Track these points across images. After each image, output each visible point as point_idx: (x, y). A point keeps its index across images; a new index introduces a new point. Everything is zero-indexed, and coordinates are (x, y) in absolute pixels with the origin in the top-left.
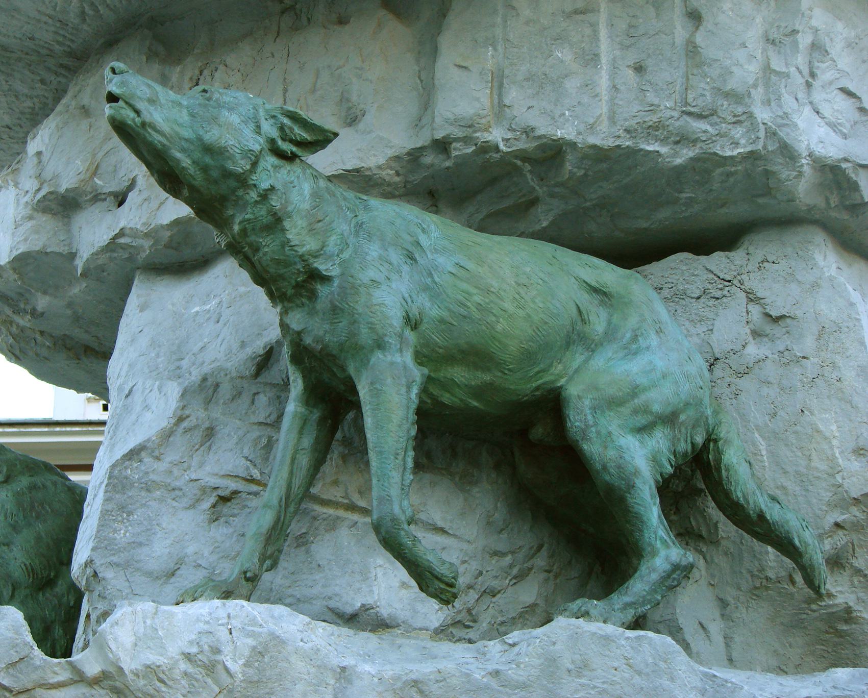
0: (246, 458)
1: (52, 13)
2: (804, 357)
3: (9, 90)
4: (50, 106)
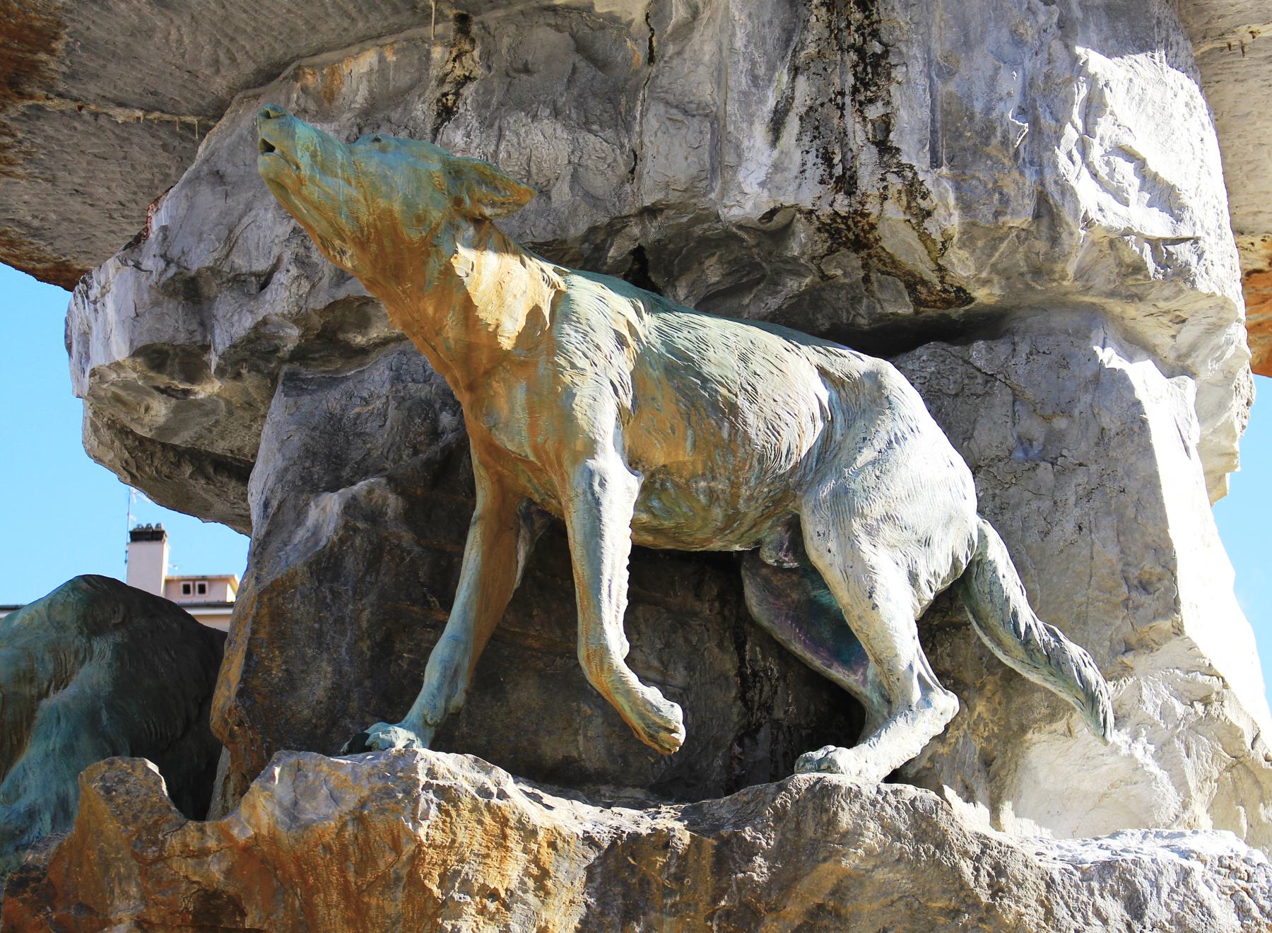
1: (180, 62)
2: (1080, 465)
3: (125, 158)
4: (173, 178)
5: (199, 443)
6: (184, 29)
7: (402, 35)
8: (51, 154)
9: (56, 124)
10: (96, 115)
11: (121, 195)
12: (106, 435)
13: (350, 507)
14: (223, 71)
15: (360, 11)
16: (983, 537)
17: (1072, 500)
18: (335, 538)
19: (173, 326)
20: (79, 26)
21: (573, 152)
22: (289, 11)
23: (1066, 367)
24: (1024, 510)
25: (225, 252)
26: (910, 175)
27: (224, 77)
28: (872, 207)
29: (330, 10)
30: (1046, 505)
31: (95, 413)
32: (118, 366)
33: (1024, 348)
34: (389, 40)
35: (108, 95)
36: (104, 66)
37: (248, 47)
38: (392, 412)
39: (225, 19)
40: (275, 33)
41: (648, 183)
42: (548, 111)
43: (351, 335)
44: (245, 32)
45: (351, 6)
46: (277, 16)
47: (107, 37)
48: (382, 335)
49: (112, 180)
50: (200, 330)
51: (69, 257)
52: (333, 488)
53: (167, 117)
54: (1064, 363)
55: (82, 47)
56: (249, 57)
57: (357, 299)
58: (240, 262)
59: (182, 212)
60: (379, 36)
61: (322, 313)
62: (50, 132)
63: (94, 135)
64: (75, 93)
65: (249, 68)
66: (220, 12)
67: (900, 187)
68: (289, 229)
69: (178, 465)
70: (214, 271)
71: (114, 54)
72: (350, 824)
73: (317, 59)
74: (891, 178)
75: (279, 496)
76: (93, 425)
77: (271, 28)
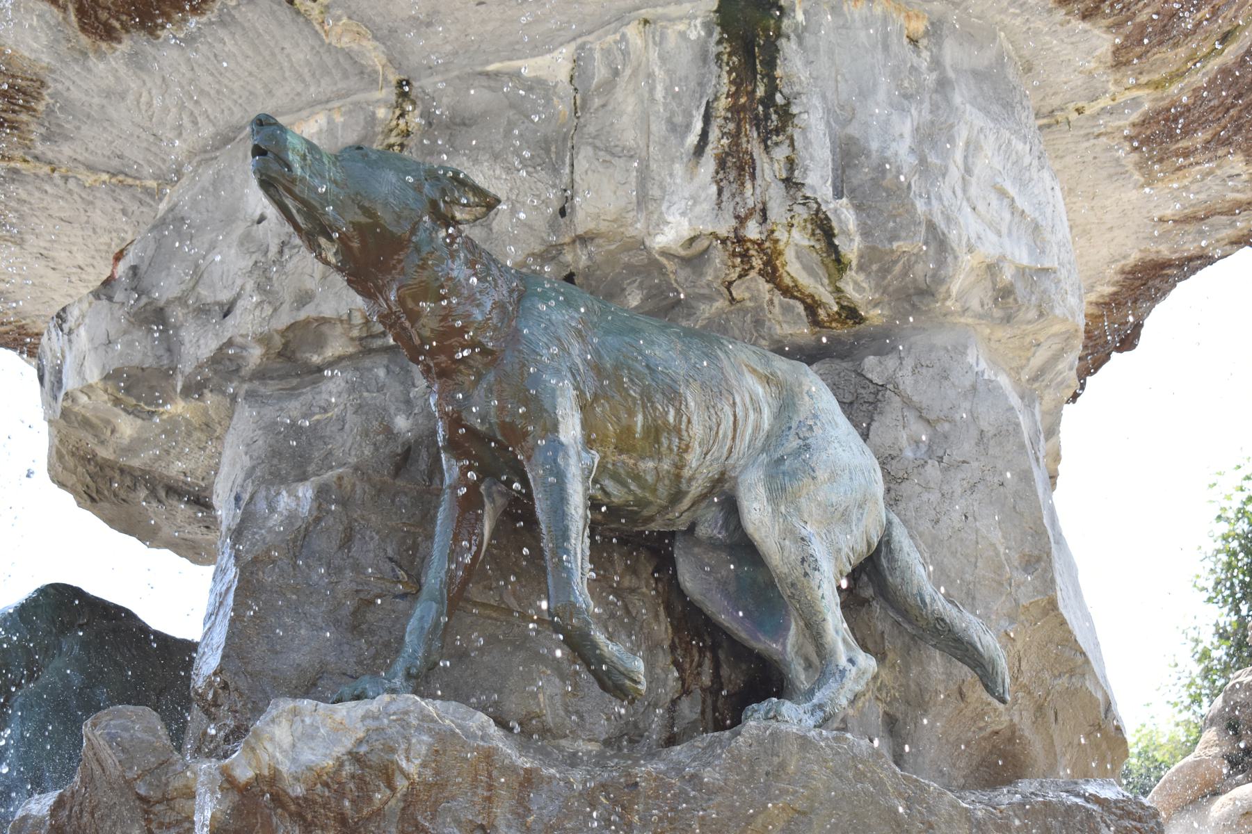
0: (391, 559)
1: (148, 124)
2: (964, 462)
3: (87, 222)
5: (156, 465)
6: (154, 92)
7: (349, 100)
8: (22, 217)
9: (29, 187)
10: (66, 179)
11: (80, 259)
12: (71, 462)
13: (322, 493)
15: (313, 75)
16: (889, 523)
17: (959, 491)
18: (310, 519)
19: (139, 350)
20: (59, 86)
21: (511, 190)
22: (251, 74)
23: (946, 378)
24: (917, 502)
25: (191, 284)
26: (815, 206)
27: (185, 141)
28: (781, 234)
29: (287, 74)
30: (934, 497)
31: (61, 441)
32: (88, 390)
33: (909, 363)
34: (336, 104)
35: (80, 158)
36: (78, 128)
37: (210, 111)
38: (350, 417)
39: (191, 82)
40: (235, 97)
41: (580, 215)
42: (487, 156)
43: (308, 355)
44: (209, 95)
45: (306, 70)
46: (240, 79)
47: (84, 98)
48: (337, 354)
49: (73, 244)
50: (167, 355)
51: (28, 321)
52: (303, 478)
53: (130, 181)
54: (944, 375)
55: (61, 108)
56: (210, 120)
57: (316, 320)
59: (150, 253)
60: (328, 101)
61: (283, 333)
62: (24, 195)
63: (62, 198)
64: (50, 155)
65: (207, 131)
66: (189, 75)
67: (805, 216)
68: (251, 263)
69: (133, 488)
70: (181, 300)
71: (89, 116)
72: (347, 763)
74: (798, 209)
75: (250, 489)
76: (59, 452)
77: (232, 91)
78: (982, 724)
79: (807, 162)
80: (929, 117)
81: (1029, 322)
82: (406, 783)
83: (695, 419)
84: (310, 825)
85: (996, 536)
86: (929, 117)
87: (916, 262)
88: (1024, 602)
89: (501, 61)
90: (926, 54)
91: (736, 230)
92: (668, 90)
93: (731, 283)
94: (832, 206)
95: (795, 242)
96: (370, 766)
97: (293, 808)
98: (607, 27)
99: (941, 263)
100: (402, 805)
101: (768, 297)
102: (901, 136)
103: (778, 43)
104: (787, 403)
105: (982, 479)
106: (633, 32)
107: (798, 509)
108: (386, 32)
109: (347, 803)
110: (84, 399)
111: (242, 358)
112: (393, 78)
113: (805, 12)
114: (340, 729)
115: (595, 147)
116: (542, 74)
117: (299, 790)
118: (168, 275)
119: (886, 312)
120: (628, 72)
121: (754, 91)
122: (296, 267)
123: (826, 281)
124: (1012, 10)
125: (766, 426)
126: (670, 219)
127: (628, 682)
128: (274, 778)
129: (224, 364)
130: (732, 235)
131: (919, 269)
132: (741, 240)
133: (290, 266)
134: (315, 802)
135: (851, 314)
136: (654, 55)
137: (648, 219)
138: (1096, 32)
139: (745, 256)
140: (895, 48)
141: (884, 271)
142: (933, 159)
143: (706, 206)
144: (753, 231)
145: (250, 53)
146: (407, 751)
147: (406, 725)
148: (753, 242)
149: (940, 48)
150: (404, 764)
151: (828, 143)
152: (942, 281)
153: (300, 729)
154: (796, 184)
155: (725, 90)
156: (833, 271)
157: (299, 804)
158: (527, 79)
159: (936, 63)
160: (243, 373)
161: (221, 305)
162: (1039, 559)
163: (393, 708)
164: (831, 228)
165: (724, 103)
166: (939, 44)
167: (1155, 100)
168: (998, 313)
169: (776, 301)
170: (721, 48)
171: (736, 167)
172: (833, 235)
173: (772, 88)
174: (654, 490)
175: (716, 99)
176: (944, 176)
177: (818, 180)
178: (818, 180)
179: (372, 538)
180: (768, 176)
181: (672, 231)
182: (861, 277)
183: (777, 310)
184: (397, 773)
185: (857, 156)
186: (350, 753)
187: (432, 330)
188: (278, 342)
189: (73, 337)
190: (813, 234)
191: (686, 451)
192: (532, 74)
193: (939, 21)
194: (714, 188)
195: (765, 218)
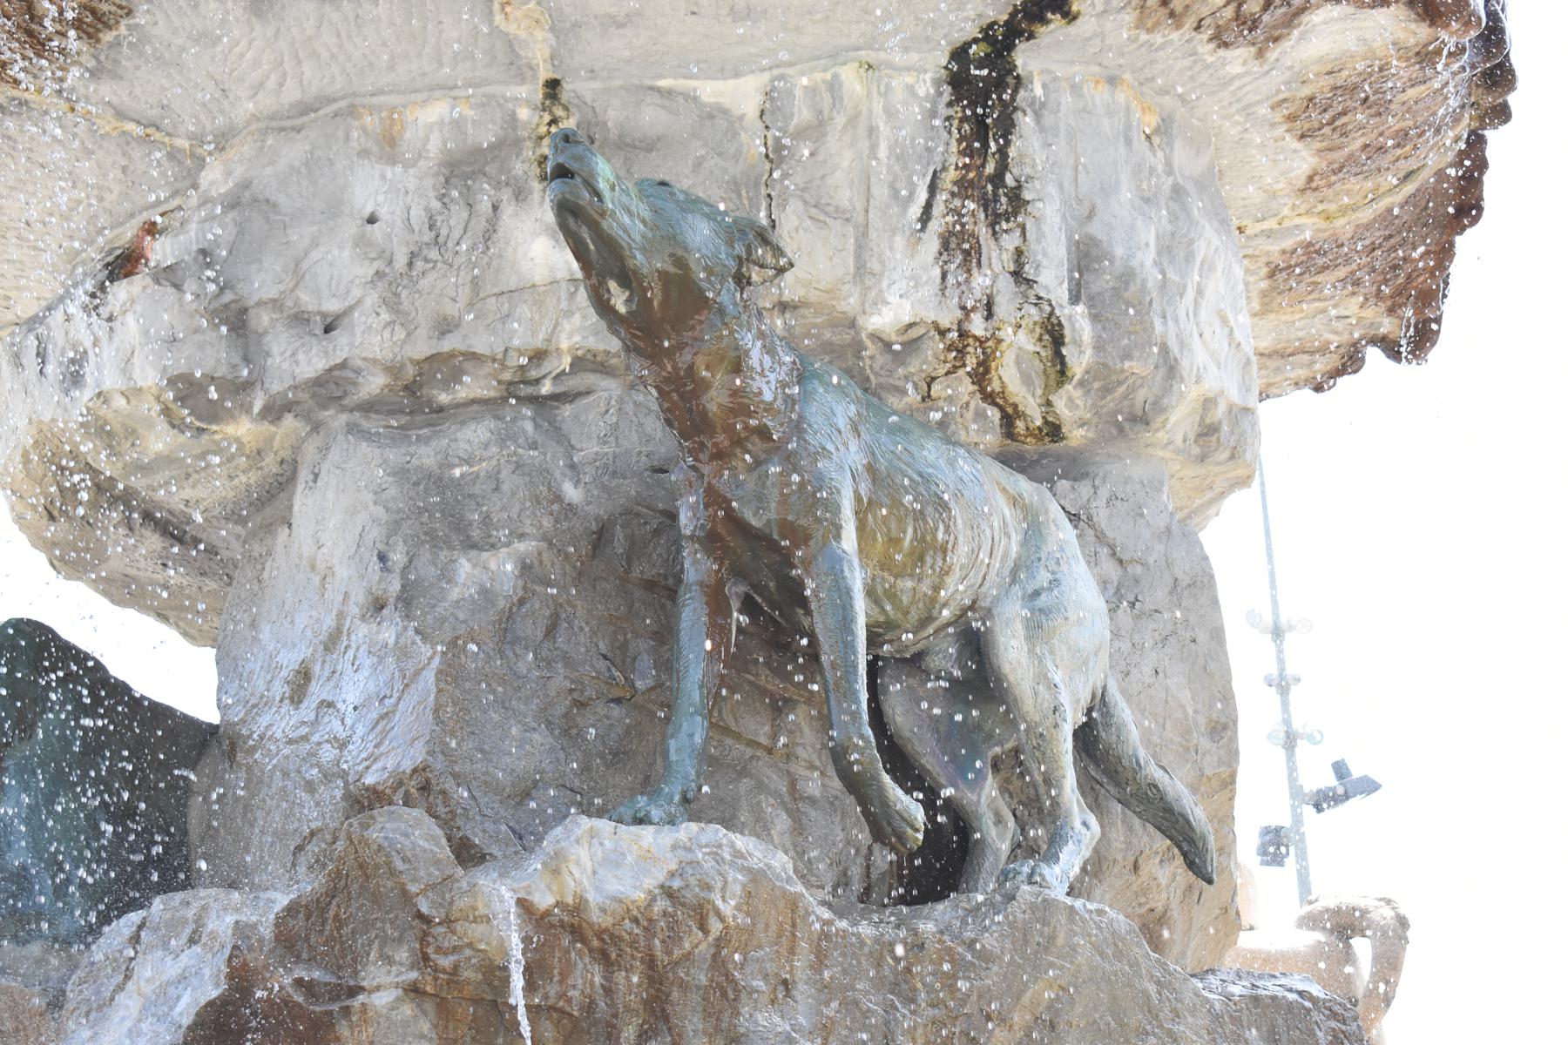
0: (605, 657)
14: (260, 97)
18: (515, 599)
19: (211, 355)
26: (1048, 309)
28: (1007, 333)
33: (1104, 493)
43: (435, 392)
48: (472, 396)
58: (307, 300)
65: (292, 94)
67: (1037, 318)
68: (371, 272)
70: (276, 304)
73: (374, 100)
78: (1143, 900)
79: (1040, 257)
80: (1169, 228)
81: (1219, 464)
82: (720, 926)
83: (961, 538)
84: (612, 964)
85: (1186, 697)
86: (1169, 228)
87: (1141, 386)
88: (1208, 772)
89: (675, 78)
90: (1160, 154)
91: (960, 323)
92: (891, 149)
93: (934, 379)
94: (1066, 311)
95: (1018, 344)
96: (685, 904)
97: (596, 943)
98: (814, 63)
99: (1167, 390)
100: (713, 951)
101: (966, 398)
102: (1147, 245)
103: (1015, 116)
104: (1034, 531)
105: (1174, 633)
106: (850, 76)
107: (1052, 652)
108: (568, 25)
109: (657, 942)
110: (120, 402)
111: (355, 384)
112: (545, 74)
113: (1044, 86)
114: (647, 858)
115: (805, 203)
116: (725, 102)
117: (606, 921)
118: (260, 270)
119: (1090, 435)
120: (840, 120)
121: (983, 166)
122: (434, 287)
123: (1039, 392)
124: (1237, 118)
125: (1013, 555)
126: (891, 299)
127: (910, 831)
128: (579, 907)
129: (330, 388)
130: (955, 327)
131: (1141, 395)
132: (963, 334)
133: (424, 283)
134: (621, 939)
135: (1053, 431)
136: (878, 107)
137: (863, 296)
138: (1304, 154)
139: (962, 352)
140: (1135, 144)
141: (1107, 390)
142: (1173, 276)
143: (930, 290)
144: (978, 326)
145: (398, 21)
146: (723, 889)
147: (719, 860)
148: (976, 338)
149: (1172, 150)
150: (719, 903)
151: (1064, 240)
152: (1163, 410)
153: (599, 853)
154: (1028, 281)
155: (953, 160)
156: (1052, 382)
157: (603, 940)
158: (705, 105)
159: (1168, 163)
160: (346, 402)
161: (324, 315)
162: (1225, 728)
163: (704, 840)
164: (1062, 336)
165: (952, 175)
166: (1170, 144)
167: (1318, 230)
168: (1196, 450)
169: (972, 405)
170: (951, 112)
171: (960, 249)
172: (1063, 344)
173: (1003, 166)
174: (906, 613)
175: (944, 169)
176: (1182, 296)
177: (1052, 279)
178: (1052, 279)
179: (581, 629)
180: (997, 267)
181: (889, 314)
182: (1077, 394)
183: (969, 415)
184: (711, 914)
185: (1100, 260)
186: (662, 887)
187: (720, 406)
188: (410, 371)
189: (116, 324)
190: (1040, 340)
191: (947, 573)
192: (712, 100)
193: (1169, 117)
194: (937, 272)
195: (989, 315)
